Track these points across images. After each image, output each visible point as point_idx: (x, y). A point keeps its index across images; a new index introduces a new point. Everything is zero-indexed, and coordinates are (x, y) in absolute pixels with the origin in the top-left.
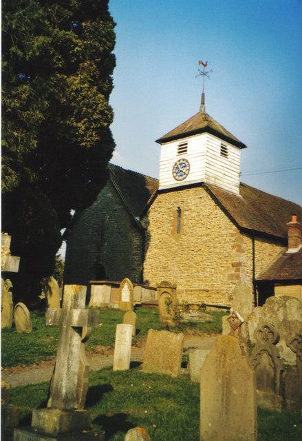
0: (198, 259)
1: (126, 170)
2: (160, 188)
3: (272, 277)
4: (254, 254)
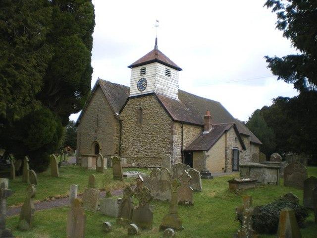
0: (151, 139)
1: (113, 84)
2: (130, 96)
3: (192, 149)
4: (182, 135)
